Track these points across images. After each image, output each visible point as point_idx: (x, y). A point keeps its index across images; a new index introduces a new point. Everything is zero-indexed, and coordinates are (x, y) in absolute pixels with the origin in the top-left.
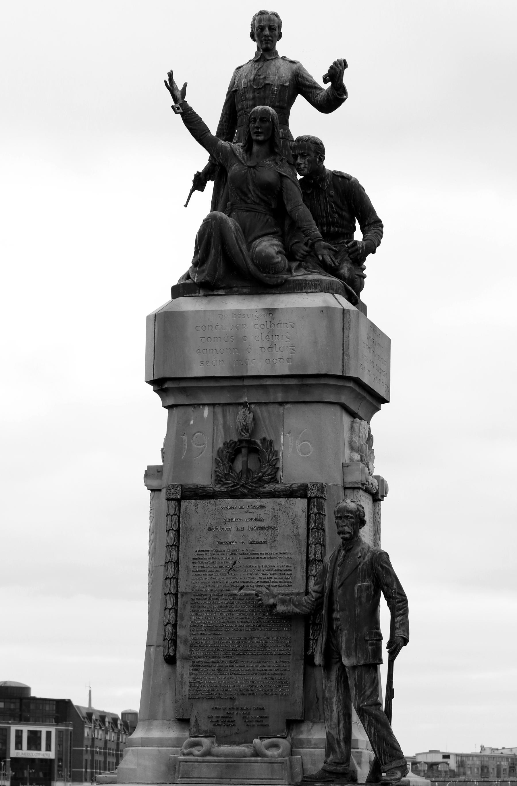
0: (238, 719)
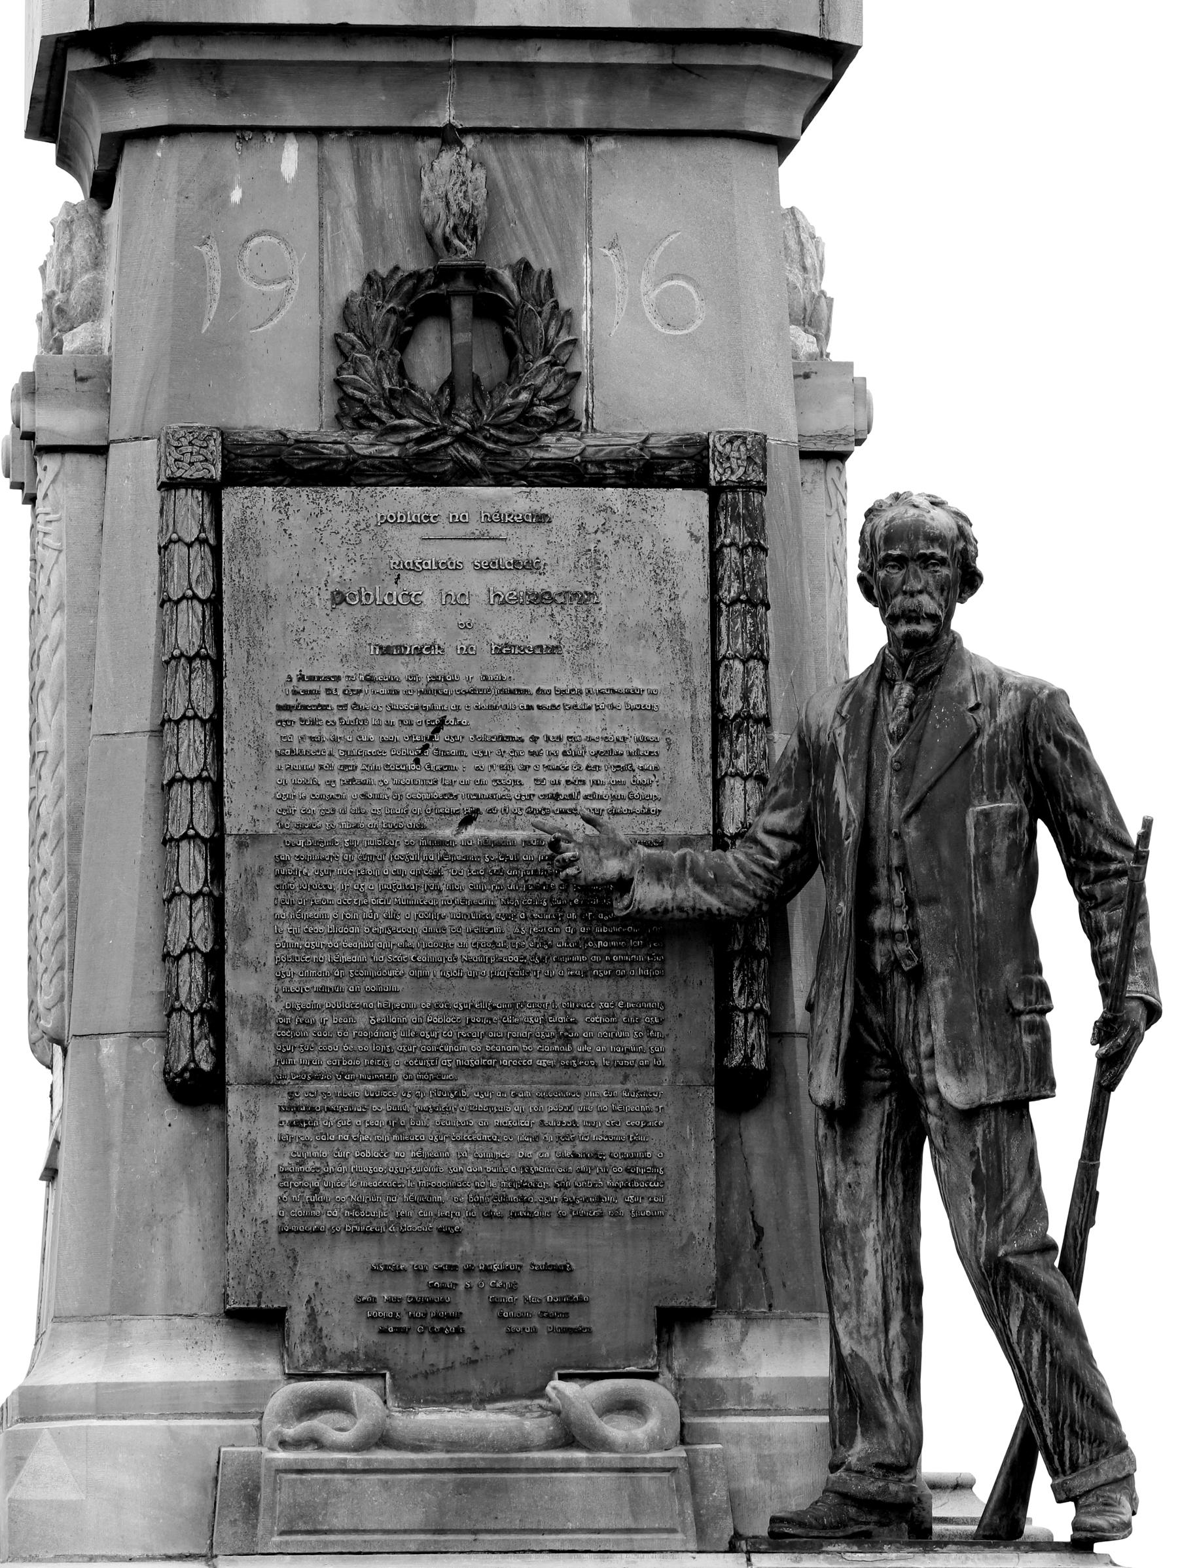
0: (470, 1305)
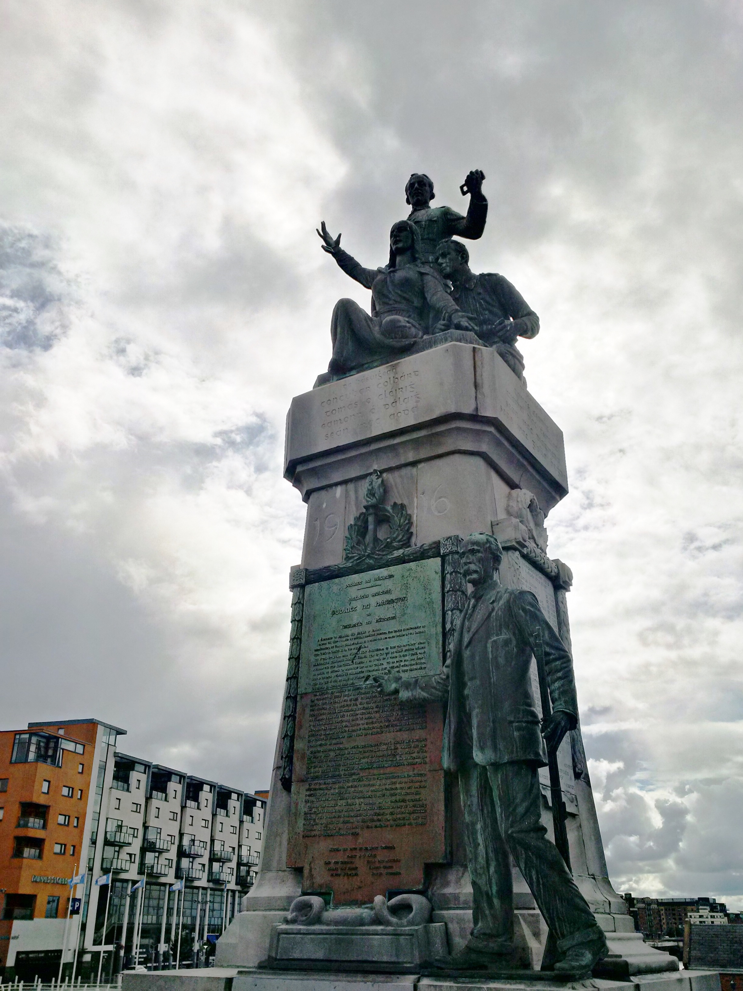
0: (360, 864)
